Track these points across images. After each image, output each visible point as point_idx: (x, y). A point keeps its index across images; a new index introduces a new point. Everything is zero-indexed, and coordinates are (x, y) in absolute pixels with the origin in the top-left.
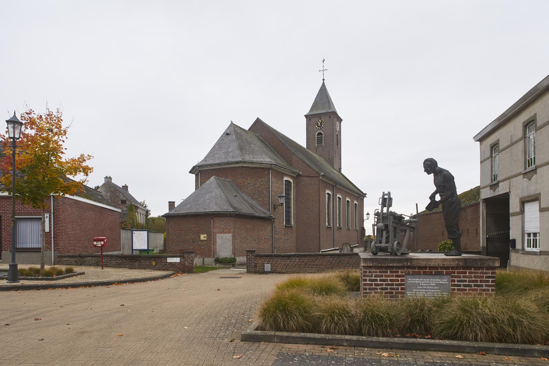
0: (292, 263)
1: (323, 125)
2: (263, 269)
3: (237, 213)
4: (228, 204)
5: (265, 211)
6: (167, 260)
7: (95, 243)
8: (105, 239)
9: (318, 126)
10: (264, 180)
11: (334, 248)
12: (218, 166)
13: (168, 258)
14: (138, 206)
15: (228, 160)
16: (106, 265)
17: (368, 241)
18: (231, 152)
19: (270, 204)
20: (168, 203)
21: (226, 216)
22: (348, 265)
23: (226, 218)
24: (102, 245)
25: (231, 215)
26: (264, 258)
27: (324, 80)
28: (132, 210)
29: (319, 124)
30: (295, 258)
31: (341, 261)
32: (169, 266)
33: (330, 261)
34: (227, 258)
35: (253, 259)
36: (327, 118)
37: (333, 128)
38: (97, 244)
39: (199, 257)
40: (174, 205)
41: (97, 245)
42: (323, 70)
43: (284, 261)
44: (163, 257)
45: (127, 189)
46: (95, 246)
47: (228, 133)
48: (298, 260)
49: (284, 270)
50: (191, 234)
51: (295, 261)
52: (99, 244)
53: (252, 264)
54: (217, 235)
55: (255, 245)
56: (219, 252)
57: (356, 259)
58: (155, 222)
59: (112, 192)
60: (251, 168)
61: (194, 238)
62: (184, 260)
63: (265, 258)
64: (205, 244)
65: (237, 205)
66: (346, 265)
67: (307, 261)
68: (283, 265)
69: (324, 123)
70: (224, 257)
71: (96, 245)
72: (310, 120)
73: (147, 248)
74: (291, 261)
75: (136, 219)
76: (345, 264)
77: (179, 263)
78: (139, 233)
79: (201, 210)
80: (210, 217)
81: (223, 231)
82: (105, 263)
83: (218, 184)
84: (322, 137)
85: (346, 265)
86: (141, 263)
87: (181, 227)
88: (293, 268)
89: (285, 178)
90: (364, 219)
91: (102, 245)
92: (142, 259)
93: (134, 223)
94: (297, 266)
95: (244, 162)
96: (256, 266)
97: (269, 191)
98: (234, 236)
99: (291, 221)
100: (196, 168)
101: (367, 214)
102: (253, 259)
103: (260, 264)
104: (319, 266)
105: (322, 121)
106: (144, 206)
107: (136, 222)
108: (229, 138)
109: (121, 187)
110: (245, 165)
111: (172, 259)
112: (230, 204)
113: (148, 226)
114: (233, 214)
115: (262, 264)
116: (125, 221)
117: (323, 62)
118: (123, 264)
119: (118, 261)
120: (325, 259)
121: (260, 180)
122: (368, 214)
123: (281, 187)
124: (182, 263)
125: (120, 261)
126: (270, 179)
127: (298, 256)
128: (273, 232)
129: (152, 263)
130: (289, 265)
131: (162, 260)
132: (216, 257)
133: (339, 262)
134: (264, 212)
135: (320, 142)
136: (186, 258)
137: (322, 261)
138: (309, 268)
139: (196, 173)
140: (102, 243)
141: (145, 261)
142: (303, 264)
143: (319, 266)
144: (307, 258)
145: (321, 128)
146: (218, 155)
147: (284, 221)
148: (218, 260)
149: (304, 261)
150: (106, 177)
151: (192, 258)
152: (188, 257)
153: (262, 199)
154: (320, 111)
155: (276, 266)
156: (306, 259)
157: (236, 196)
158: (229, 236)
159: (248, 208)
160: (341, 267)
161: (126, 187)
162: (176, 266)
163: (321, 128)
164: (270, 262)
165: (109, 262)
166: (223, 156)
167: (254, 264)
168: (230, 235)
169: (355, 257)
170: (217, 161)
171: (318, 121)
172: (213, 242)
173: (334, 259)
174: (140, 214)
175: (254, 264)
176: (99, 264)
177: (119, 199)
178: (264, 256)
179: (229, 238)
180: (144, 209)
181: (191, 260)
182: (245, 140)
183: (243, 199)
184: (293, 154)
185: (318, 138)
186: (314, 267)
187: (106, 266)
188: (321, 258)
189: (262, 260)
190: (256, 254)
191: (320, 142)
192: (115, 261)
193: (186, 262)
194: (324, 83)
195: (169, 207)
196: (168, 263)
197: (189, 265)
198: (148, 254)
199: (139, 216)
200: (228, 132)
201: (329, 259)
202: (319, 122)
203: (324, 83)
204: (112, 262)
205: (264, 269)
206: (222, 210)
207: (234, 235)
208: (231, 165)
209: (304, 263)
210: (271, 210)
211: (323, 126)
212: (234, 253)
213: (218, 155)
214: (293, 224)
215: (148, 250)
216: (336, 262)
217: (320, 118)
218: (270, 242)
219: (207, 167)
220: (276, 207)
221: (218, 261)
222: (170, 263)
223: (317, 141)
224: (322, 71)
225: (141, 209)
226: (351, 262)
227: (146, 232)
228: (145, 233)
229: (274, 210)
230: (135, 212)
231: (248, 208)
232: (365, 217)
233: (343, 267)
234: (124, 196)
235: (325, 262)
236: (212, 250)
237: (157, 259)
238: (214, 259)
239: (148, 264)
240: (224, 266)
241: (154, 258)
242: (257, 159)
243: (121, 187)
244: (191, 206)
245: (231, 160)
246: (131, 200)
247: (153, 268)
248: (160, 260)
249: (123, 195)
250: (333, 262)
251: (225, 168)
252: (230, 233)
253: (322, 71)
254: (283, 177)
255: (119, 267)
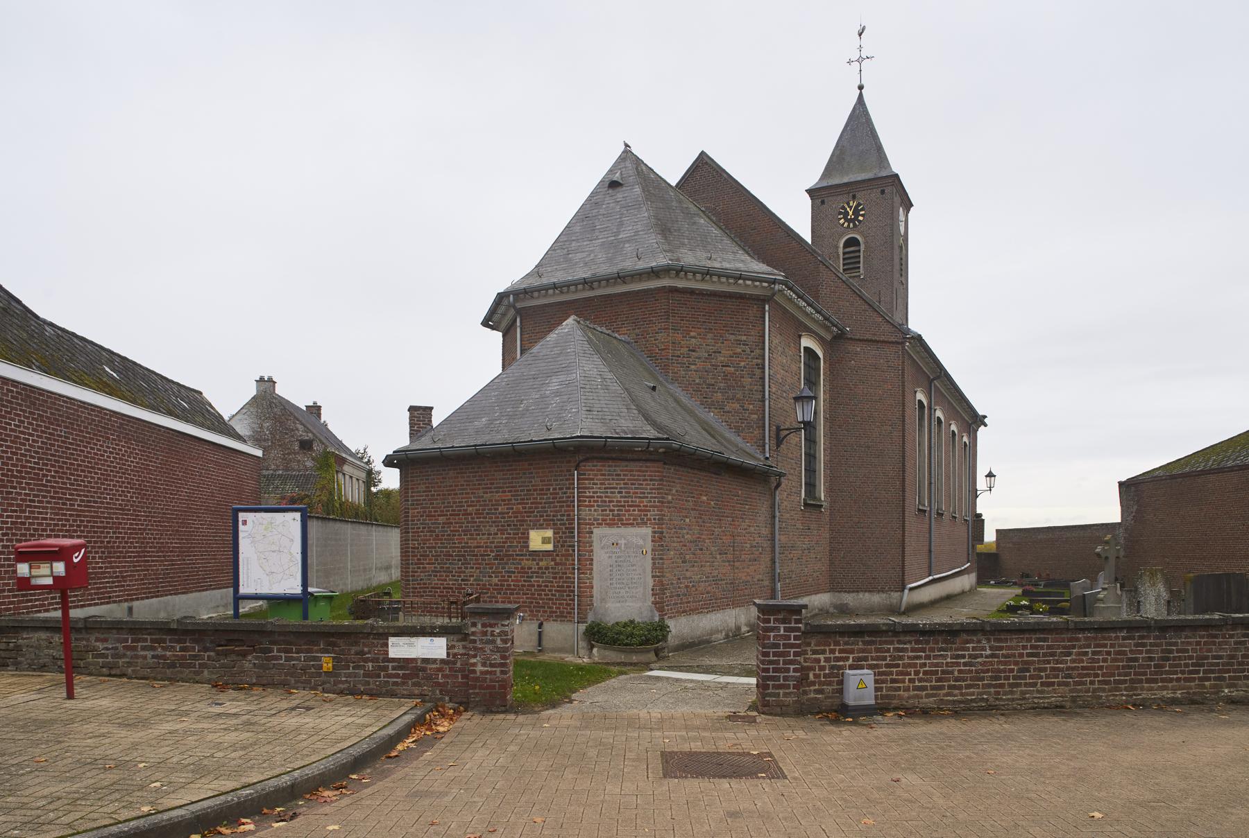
0: (965, 664)
1: (862, 215)
2: (834, 691)
3: (675, 445)
4: (636, 412)
5: (748, 447)
6: (387, 645)
7: (23, 569)
8: (77, 548)
9: (846, 220)
10: (744, 338)
11: (931, 578)
12: (584, 289)
13: (392, 640)
14: (344, 455)
15: (620, 267)
16: (111, 668)
17: (1107, 558)
18: (628, 241)
19: (764, 424)
20: (408, 414)
21: (629, 456)
22: (1198, 672)
23: (632, 463)
24: (56, 579)
25: (651, 453)
26: (842, 640)
27: (861, 88)
28: (329, 466)
29: (851, 213)
30: (979, 642)
31: (1171, 652)
32: (397, 676)
33: (1124, 653)
34: (632, 622)
35: (792, 646)
36: (875, 194)
37: (892, 225)
38: (35, 572)
39: (523, 619)
40: (431, 421)
41: (33, 582)
42: (860, 60)
43: (928, 657)
44: (369, 634)
45: (319, 415)
46: (24, 583)
47: (615, 179)
48: (988, 652)
49: (928, 696)
50: (494, 529)
51: (976, 657)
52: (45, 574)
53: (788, 670)
54: (595, 531)
55: (724, 571)
56: (603, 600)
57: (1236, 643)
58: (392, 501)
59: (276, 419)
60: (701, 293)
61: (506, 542)
62: (464, 647)
63: (846, 643)
64: (547, 568)
65: (664, 419)
66: (1191, 672)
67: (1029, 655)
68: (925, 673)
69: (867, 217)
70: (625, 619)
71: (27, 580)
72: (823, 202)
73: (297, 589)
74: (958, 657)
75: (339, 490)
76: (1187, 665)
77: (442, 661)
78: (265, 522)
79: (532, 432)
80: (569, 462)
81: (619, 515)
82: (110, 659)
83: (590, 341)
84: (859, 251)
85: (1191, 672)
86: (268, 659)
87: (454, 503)
88: (968, 687)
89: (806, 342)
90: (977, 490)
91: (56, 579)
92: (274, 643)
93: (333, 499)
94: (982, 679)
95: (679, 271)
96: (802, 681)
97: (763, 378)
98: (658, 538)
99: (817, 488)
100: (505, 302)
101: (986, 476)
102: (792, 646)
103: (822, 668)
104: (1080, 675)
105: (859, 204)
106: (366, 460)
107: (339, 498)
108: (619, 196)
109: (322, 421)
110: (681, 284)
111: (411, 645)
112: (640, 411)
113: (372, 510)
114: (656, 451)
115: (832, 667)
116: (307, 496)
117: (860, 35)
118: (190, 666)
119: (164, 649)
120: (1105, 646)
121: (732, 337)
122: (990, 475)
123: (794, 367)
124: (458, 665)
125: (174, 651)
126: (764, 337)
127: (992, 632)
128: (774, 524)
129: (319, 659)
130: (952, 672)
131: (364, 645)
132: (590, 618)
133: (1163, 659)
134: (748, 450)
135: (851, 266)
136: (475, 641)
137: (1094, 653)
138: (1035, 685)
139: (504, 324)
140: (59, 568)
141: (286, 651)
142: (1012, 671)
143: (1080, 675)
144: (1029, 640)
145: (855, 224)
146: (584, 255)
147: (801, 485)
148: (598, 632)
149: (1014, 655)
150: (262, 379)
151: (505, 642)
152: (485, 633)
153: (737, 406)
154: (851, 176)
155: (893, 681)
156: (1024, 647)
157: (654, 388)
158: (641, 536)
159: (699, 432)
160: (1171, 680)
161: (315, 410)
162: (429, 678)
163: (855, 225)
164: (866, 659)
165: (124, 656)
166: (601, 257)
167: (795, 670)
168: (647, 531)
169: (1232, 636)
170: (582, 273)
171: (848, 204)
172: (579, 560)
173: (1144, 645)
174: (351, 477)
175: (795, 670)
176: (82, 663)
177: (293, 436)
178: (842, 634)
179: (641, 542)
180: (366, 466)
181: (498, 650)
182: (674, 204)
183: (677, 401)
184: (822, 268)
185: (847, 256)
186: (1059, 684)
187: (113, 672)
188: (1087, 638)
189: (832, 652)
190: (806, 624)
191: (851, 266)
192: (153, 649)
193: (473, 661)
194: (861, 96)
195: (412, 425)
196: (394, 660)
197: (491, 673)
198: (305, 617)
199: (347, 485)
200: (617, 177)
201: (1120, 646)
202: (851, 208)
203: (861, 96)
204: (137, 657)
205: (841, 691)
206: (617, 433)
207: (662, 533)
208: (632, 282)
209: (1016, 663)
210: (767, 446)
211: (861, 218)
212: (659, 605)
213: (584, 255)
214: (823, 499)
215: (303, 601)
216: (1151, 659)
217: (854, 197)
218: (766, 559)
219: (546, 296)
220: (782, 437)
221: (597, 635)
222: (404, 663)
223: (844, 265)
224: (858, 61)
225: (353, 464)
226: (1215, 657)
227: (298, 515)
228: (291, 522)
229: (778, 445)
230: (337, 472)
231: (699, 432)
232: (981, 483)
233: (1178, 680)
234: (307, 430)
235: (1105, 660)
236: (574, 591)
237: (340, 642)
238: (583, 627)
239: (300, 664)
240: (622, 657)
241: (329, 637)
242: (721, 262)
243: (305, 409)
244: (491, 422)
245: (629, 264)
246: (325, 441)
247: (324, 683)
248: (354, 649)
249: (305, 426)
250: (1136, 660)
251: (609, 296)
252: (644, 524)
253: (858, 61)
254: (800, 337)
255: (172, 680)
